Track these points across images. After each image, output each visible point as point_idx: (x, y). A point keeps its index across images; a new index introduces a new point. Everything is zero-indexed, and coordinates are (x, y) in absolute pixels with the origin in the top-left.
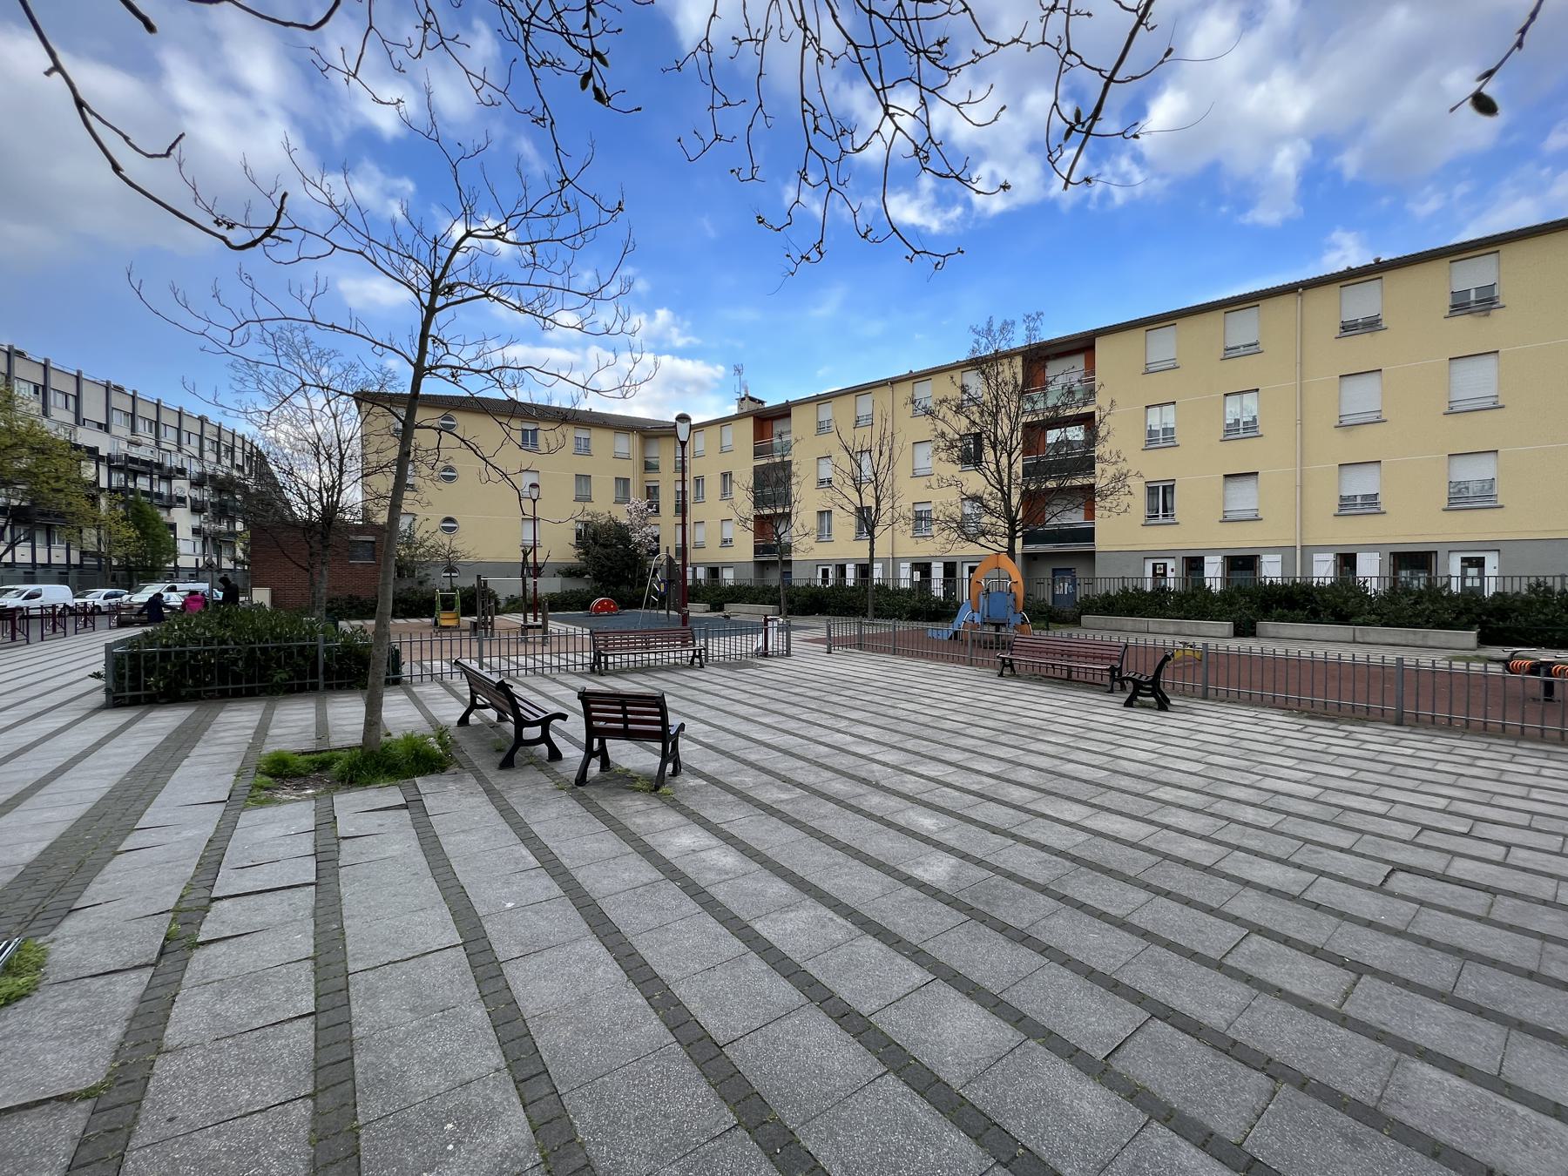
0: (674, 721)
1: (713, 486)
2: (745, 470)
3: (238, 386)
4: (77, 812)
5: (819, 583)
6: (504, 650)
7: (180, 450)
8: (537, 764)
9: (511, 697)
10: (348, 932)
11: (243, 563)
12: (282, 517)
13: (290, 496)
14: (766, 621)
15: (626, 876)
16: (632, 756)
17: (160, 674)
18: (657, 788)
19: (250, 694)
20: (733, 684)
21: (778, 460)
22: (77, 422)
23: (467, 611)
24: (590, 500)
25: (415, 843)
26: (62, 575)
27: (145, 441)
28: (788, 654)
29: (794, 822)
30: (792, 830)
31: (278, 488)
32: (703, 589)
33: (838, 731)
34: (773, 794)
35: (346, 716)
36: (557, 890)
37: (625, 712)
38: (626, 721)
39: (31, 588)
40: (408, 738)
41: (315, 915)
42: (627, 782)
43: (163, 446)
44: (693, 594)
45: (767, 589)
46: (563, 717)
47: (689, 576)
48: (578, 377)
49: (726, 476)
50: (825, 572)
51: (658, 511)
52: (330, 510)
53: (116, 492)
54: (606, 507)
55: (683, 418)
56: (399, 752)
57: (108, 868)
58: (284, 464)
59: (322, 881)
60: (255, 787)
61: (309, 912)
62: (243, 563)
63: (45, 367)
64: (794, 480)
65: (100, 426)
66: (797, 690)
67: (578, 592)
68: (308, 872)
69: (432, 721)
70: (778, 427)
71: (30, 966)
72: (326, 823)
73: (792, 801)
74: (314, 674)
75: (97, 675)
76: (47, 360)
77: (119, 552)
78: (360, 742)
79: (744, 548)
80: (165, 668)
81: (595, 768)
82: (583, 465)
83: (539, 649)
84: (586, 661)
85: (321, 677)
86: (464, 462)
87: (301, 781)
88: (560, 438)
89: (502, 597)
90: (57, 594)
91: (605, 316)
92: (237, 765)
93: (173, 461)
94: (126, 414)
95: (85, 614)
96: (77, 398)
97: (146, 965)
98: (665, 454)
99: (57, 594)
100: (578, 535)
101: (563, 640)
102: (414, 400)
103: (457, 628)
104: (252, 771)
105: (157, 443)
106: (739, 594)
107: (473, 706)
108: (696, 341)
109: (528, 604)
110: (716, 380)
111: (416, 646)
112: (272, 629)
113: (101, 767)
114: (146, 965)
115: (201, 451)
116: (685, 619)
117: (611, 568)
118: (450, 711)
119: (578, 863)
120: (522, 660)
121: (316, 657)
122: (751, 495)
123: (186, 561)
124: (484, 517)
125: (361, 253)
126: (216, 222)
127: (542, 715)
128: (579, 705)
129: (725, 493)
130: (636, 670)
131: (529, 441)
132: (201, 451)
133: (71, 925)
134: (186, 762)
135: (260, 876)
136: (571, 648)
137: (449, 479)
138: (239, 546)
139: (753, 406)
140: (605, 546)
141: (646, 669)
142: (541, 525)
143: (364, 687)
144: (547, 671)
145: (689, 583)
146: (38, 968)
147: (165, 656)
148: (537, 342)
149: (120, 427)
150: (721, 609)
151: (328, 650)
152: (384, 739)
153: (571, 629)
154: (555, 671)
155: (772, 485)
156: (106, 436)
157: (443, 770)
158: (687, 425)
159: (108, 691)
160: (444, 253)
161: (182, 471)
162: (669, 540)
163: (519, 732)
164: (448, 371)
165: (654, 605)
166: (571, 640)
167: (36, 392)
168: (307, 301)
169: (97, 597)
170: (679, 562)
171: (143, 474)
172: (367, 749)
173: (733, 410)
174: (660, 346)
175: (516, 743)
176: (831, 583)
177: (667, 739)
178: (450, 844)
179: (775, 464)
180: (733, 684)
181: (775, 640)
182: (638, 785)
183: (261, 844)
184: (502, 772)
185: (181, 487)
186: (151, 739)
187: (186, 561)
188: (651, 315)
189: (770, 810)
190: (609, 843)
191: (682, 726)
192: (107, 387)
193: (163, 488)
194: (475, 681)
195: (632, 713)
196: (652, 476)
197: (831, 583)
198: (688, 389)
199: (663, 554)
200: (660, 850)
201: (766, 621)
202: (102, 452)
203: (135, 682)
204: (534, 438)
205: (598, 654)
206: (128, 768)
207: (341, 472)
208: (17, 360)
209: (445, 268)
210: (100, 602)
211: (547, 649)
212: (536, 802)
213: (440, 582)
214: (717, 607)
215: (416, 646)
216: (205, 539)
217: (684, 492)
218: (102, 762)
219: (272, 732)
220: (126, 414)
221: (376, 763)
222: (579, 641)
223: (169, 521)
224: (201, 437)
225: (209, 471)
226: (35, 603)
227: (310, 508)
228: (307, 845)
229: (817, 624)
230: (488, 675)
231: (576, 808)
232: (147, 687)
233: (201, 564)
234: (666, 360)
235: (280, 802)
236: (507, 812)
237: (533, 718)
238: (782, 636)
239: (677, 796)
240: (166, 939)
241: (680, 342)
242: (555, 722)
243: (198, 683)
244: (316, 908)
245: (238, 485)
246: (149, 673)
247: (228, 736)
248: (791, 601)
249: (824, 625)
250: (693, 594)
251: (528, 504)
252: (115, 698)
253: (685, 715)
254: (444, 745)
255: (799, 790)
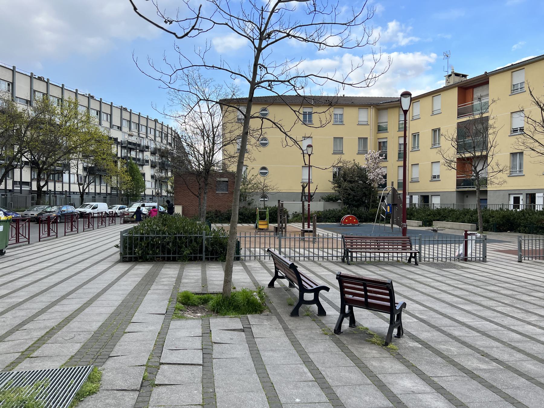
0: (399, 300)
1: (426, 139)
2: (450, 125)
3: (170, 103)
4: (111, 310)
5: (511, 208)
6: (292, 244)
7: (147, 137)
8: (310, 315)
9: (298, 274)
10: (217, 394)
11: (171, 193)
12: (187, 169)
13: (191, 158)
14: (466, 235)
15: (367, 398)
16: (371, 320)
17: (142, 248)
18: (386, 344)
19: (174, 260)
20: (440, 278)
21: (477, 117)
22: (111, 127)
23: (273, 220)
24: (342, 153)
25: (248, 353)
26: (104, 197)
27: (135, 134)
28: (484, 260)
29: (491, 387)
30: (489, 392)
31: (186, 154)
32: (417, 211)
33: (529, 323)
34: (473, 363)
35: (215, 274)
36: (324, 398)
37: (366, 291)
38: (366, 297)
39: (94, 204)
40: (244, 291)
41: (202, 382)
42: (367, 337)
43: (141, 135)
44: (410, 214)
45: (467, 212)
46: (327, 289)
47: (408, 201)
48: (338, 76)
49: (436, 131)
50: (517, 200)
51: (386, 158)
52: (209, 164)
53: (123, 159)
54: (352, 157)
55: (406, 94)
56: (240, 298)
57: (122, 339)
58: (189, 141)
59: (205, 364)
60: (176, 308)
61: (200, 379)
62: (171, 193)
63: (62, 88)
64: (490, 131)
65: (118, 127)
66: (492, 288)
67: (334, 211)
68: (198, 358)
69: (255, 283)
70: (478, 93)
71: (97, 380)
72: (207, 333)
73: (489, 371)
74: (201, 252)
75: (117, 246)
76: (14, 67)
77: (124, 187)
78: (221, 291)
79: (449, 182)
80: (141, 244)
81: (346, 324)
82: (338, 131)
83: (311, 245)
84: (339, 254)
85: (204, 253)
86: (273, 136)
87: (195, 308)
88: (328, 117)
89: (290, 213)
90: (103, 207)
91: (356, 34)
92: (169, 296)
93: (144, 143)
94: (128, 121)
95: (112, 217)
96: (111, 115)
97: (136, 390)
98: (392, 120)
99: (103, 207)
100: (335, 175)
101: (325, 240)
102: (251, 101)
103: (267, 230)
104: (175, 300)
105: (139, 135)
106: (443, 215)
107: (276, 277)
108: (416, 39)
109: (306, 217)
110: (429, 64)
111: (248, 239)
112: (184, 227)
113: (118, 290)
114: (136, 390)
115: (155, 136)
116: (405, 231)
117: (354, 196)
118: (265, 278)
119: (337, 383)
120: (302, 251)
121: (202, 243)
122: (455, 144)
123: (148, 192)
124: (288, 165)
125: (226, 24)
126: (166, 22)
127: (315, 287)
128: (336, 283)
129: (435, 143)
130: (371, 263)
131: (307, 119)
132: (155, 136)
133: (110, 363)
134: (149, 292)
135: (179, 356)
136: (330, 246)
137: (264, 145)
138: (169, 184)
139: (458, 79)
140: (351, 182)
141: (377, 263)
142: (313, 170)
143: (224, 260)
144: (316, 259)
145: (408, 206)
146: (99, 381)
147: (142, 239)
148: (313, 56)
149: (125, 129)
150: (430, 225)
151: (207, 239)
152: (232, 290)
153: (330, 234)
154: (321, 259)
155: (472, 137)
156: (120, 132)
157: (261, 312)
158: (409, 99)
159: (121, 254)
160: (266, 15)
161: (147, 147)
162: (394, 176)
163: (301, 296)
164: (267, 83)
165: (383, 220)
166: (330, 241)
167: (97, 114)
168: (202, 55)
169: (116, 209)
170: (400, 192)
171: (133, 149)
172: (225, 295)
173: (442, 84)
174: (390, 47)
175: (302, 302)
176: (521, 208)
177: (394, 313)
178: (266, 356)
179: (476, 120)
180: (440, 278)
181: (473, 249)
182: (374, 340)
183: (179, 339)
184: (292, 318)
185: (147, 155)
186: (136, 279)
187: (148, 192)
188: (385, 27)
189: (471, 375)
190: (356, 376)
191: (404, 305)
192: (31, 77)
193: (140, 156)
194: (278, 262)
195: (371, 292)
196: (382, 135)
197: (521, 208)
198: (409, 73)
199: (389, 187)
200: (390, 386)
201: (466, 235)
202: (119, 140)
203: (133, 251)
204: (310, 117)
205: (346, 252)
206: (128, 292)
207: (214, 144)
208: (91, 100)
209: (267, 24)
210: (117, 211)
211: (316, 245)
212: (311, 339)
213: (258, 204)
214: (428, 223)
215: (248, 239)
216: (156, 181)
217: (405, 144)
218: (119, 288)
219: (184, 281)
220: (128, 121)
221: (229, 304)
222: (335, 241)
223: (142, 172)
224: (155, 130)
225: (158, 147)
226: (95, 211)
227: (200, 164)
228: (198, 344)
229: (508, 239)
230: (284, 259)
231: (335, 348)
232: (135, 253)
233: (154, 194)
234: (394, 55)
235: (187, 319)
236: (295, 343)
237: (309, 288)
238: (480, 246)
239: (401, 352)
240: (143, 379)
241: (404, 42)
242: (322, 292)
243: (154, 253)
244: (203, 378)
245: (170, 153)
246: (136, 247)
247: (165, 281)
248: (487, 221)
249: (516, 240)
250: (410, 214)
251: (307, 157)
252: (123, 258)
253: (405, 297)
254: (261, 298)
255: (494, 364)
